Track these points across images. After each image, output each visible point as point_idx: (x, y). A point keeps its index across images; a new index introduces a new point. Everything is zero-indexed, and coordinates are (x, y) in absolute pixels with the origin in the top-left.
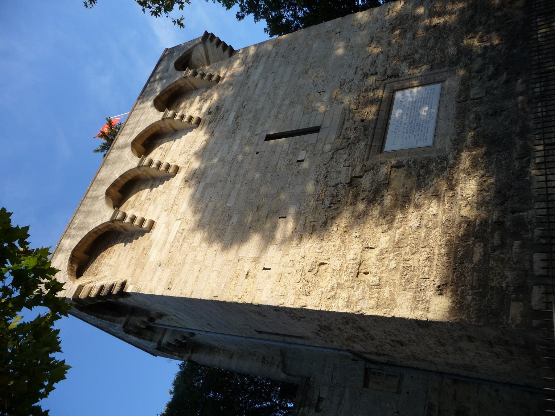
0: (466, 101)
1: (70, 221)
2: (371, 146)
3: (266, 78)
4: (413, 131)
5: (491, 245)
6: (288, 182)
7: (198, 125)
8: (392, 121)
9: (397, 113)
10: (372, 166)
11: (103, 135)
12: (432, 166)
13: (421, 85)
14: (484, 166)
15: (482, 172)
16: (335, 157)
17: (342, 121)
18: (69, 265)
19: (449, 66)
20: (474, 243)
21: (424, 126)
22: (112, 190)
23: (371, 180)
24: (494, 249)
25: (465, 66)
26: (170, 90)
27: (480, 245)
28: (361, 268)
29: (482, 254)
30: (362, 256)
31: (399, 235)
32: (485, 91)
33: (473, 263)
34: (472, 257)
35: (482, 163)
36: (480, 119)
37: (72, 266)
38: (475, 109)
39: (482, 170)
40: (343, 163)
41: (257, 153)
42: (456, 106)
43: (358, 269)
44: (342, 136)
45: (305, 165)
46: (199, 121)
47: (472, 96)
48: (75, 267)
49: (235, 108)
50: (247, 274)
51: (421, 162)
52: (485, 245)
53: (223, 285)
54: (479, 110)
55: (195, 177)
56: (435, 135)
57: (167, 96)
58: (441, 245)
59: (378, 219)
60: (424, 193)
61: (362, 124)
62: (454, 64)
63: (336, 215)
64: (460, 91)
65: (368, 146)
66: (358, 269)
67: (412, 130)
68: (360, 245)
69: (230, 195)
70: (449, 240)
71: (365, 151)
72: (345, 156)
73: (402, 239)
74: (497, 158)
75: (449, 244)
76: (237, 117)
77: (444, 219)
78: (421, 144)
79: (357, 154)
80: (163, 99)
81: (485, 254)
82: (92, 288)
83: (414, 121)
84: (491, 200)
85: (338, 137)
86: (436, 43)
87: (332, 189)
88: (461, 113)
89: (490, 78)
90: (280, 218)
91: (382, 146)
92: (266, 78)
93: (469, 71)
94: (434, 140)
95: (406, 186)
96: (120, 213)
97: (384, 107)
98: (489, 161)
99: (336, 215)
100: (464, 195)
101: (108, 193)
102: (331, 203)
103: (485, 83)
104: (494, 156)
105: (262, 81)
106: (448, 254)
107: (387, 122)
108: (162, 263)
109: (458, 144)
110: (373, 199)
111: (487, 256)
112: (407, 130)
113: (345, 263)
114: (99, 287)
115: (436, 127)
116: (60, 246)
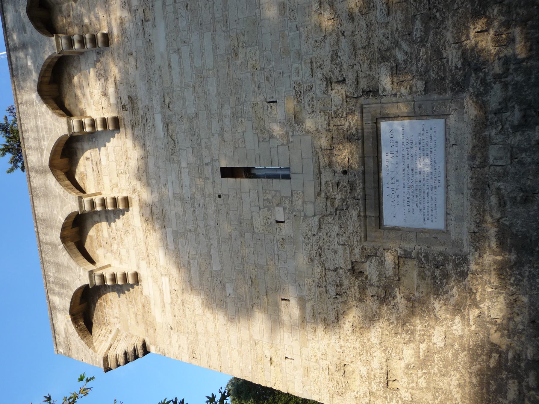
0: (483, 167)
1: (43, 273)
2: (365, 217)
3: (178, 51)
4: (417, 201)
5: (526, 384)
6: (276, 252)
7: (119, 128)
8: (384, 174)
9: (387, 158)
10: (374, 251)
11: (6, 149)
12: (450, 267)
13: (413, 116)
14: (514, 281)
15: (512, 288)
16: (323, 227)
17: (317, 168)
18: (76, 328)
19: (452, 90)
20: (507, 378)
21: (430, 195)
22: (66, 233)
23: (378, 273)
24: (529, 389)
25: (477, 96)
26: (49, 66)
27: (514, 383)
28: (389, 377)
29: (517, 393)
30: (387, 366)
31: (424, 351)
32: (509, 154)
33: (507, 400)
34: (506, 393)
35: (511, 275)
36: (505, 205)
37: (79, 326)
38: (497, 184)
39: (512, 285)
40: (336, 239)
41: (220, 196)
42: (470, 174)
43: (387, 378)
44: (323, 195)
45: (286, 229)
46: (116, 121)
47: (491, 161)
48: (82, 323)
49: (156, 98)
50: (271, 360)
51: (434, 259)
52: (520, 383)
53: (250, 367)
54: (502, 187)
55: (155, 214)
56: (447, 214)
57: (49, 74)
58: (471, 373)
59: (396, 326)
60: (445, 304)
61: (345, 178)
62: (459, 87)
63: (346, 309)
64: (474, 147)
65: (362, 219)
66: (387, 378)
67: (415, 199)
68: (383, 355)
69: (211, 255)
70: (480, 370)
71: (360, 226)
72: (337, 228)
73: (427, 356)
74: (530, 272)
75: (480, 373)
76: (167, 125)
77: (471, 343)
78: (429, 225)
79: (351, 228)
80: (47, 79)
81: (520, 393)
82: (116, 357)
83: (415, 185)
84: (523, 330)
85: (319, 194)
86: (426, 31)
87: (333, 274)
88: (480, 189)
89: (516, 129)
90: (283, 300)
91: (379, 217)
92: (178, 51)
93: (482, 106)
94: (446, 220)
95: (421, 290)
96: (97, 278)
97: (369, 144)
98: (520, 274)
99: (346, 309)
100: (492, 317)
101: (64, 238)
102: (337, 294)
103: (508, 137)
104: (526, 268)
105: (174, 58)
106: (481, 384)
107: (379, 175)
108: (172, 326)
109: (478, 238)
110: (385, 297)
111: (522, 395)
112: (408, 198)
113: (372, 370)
114: (123, 355)
115: (447, 199)
116: (51, 303)
